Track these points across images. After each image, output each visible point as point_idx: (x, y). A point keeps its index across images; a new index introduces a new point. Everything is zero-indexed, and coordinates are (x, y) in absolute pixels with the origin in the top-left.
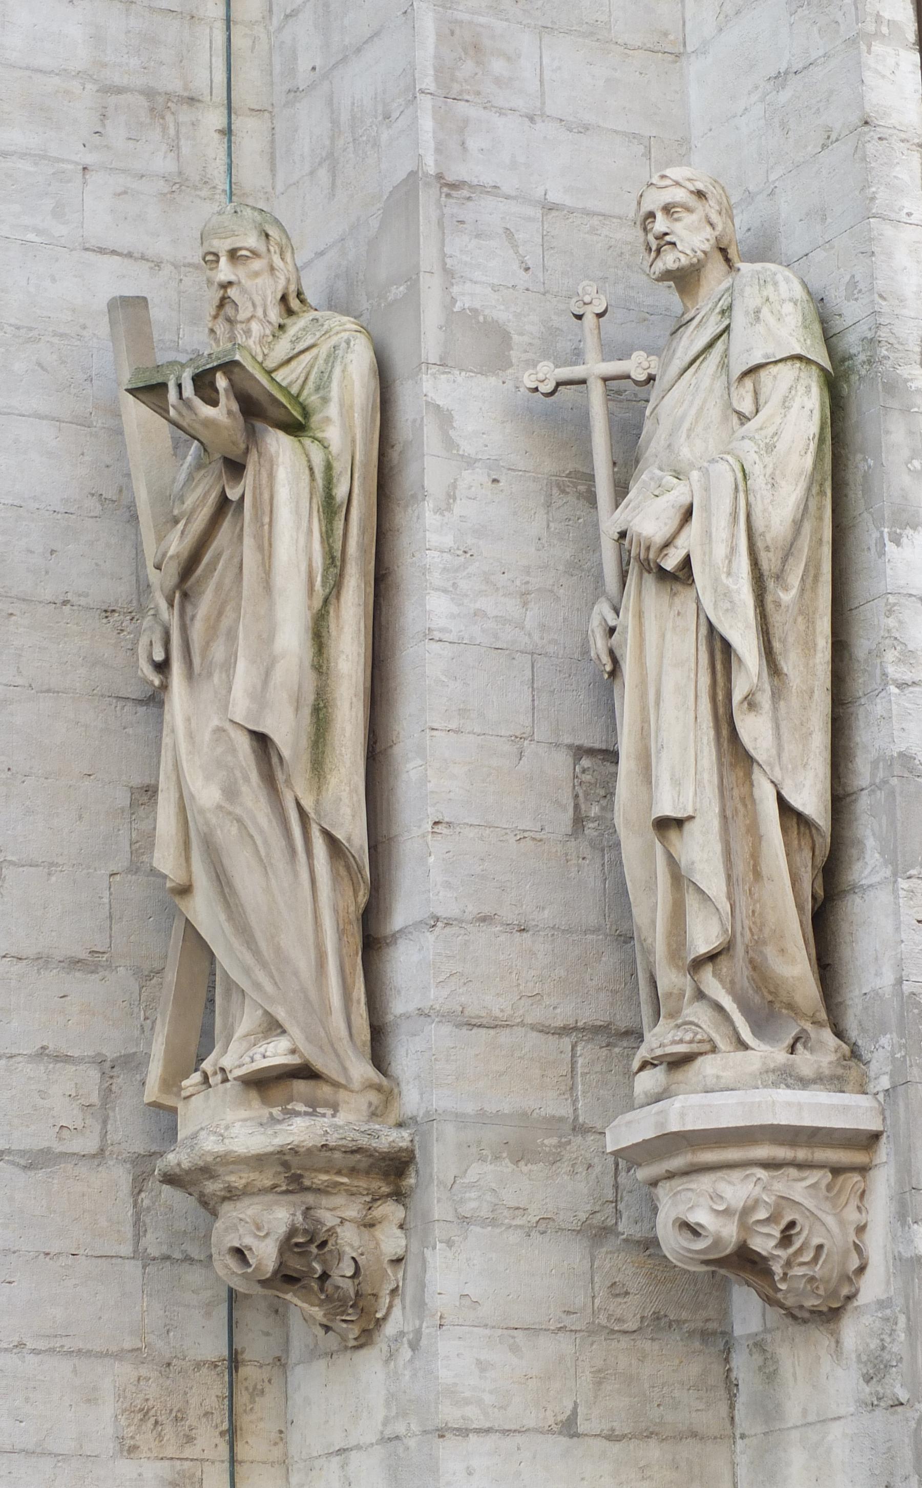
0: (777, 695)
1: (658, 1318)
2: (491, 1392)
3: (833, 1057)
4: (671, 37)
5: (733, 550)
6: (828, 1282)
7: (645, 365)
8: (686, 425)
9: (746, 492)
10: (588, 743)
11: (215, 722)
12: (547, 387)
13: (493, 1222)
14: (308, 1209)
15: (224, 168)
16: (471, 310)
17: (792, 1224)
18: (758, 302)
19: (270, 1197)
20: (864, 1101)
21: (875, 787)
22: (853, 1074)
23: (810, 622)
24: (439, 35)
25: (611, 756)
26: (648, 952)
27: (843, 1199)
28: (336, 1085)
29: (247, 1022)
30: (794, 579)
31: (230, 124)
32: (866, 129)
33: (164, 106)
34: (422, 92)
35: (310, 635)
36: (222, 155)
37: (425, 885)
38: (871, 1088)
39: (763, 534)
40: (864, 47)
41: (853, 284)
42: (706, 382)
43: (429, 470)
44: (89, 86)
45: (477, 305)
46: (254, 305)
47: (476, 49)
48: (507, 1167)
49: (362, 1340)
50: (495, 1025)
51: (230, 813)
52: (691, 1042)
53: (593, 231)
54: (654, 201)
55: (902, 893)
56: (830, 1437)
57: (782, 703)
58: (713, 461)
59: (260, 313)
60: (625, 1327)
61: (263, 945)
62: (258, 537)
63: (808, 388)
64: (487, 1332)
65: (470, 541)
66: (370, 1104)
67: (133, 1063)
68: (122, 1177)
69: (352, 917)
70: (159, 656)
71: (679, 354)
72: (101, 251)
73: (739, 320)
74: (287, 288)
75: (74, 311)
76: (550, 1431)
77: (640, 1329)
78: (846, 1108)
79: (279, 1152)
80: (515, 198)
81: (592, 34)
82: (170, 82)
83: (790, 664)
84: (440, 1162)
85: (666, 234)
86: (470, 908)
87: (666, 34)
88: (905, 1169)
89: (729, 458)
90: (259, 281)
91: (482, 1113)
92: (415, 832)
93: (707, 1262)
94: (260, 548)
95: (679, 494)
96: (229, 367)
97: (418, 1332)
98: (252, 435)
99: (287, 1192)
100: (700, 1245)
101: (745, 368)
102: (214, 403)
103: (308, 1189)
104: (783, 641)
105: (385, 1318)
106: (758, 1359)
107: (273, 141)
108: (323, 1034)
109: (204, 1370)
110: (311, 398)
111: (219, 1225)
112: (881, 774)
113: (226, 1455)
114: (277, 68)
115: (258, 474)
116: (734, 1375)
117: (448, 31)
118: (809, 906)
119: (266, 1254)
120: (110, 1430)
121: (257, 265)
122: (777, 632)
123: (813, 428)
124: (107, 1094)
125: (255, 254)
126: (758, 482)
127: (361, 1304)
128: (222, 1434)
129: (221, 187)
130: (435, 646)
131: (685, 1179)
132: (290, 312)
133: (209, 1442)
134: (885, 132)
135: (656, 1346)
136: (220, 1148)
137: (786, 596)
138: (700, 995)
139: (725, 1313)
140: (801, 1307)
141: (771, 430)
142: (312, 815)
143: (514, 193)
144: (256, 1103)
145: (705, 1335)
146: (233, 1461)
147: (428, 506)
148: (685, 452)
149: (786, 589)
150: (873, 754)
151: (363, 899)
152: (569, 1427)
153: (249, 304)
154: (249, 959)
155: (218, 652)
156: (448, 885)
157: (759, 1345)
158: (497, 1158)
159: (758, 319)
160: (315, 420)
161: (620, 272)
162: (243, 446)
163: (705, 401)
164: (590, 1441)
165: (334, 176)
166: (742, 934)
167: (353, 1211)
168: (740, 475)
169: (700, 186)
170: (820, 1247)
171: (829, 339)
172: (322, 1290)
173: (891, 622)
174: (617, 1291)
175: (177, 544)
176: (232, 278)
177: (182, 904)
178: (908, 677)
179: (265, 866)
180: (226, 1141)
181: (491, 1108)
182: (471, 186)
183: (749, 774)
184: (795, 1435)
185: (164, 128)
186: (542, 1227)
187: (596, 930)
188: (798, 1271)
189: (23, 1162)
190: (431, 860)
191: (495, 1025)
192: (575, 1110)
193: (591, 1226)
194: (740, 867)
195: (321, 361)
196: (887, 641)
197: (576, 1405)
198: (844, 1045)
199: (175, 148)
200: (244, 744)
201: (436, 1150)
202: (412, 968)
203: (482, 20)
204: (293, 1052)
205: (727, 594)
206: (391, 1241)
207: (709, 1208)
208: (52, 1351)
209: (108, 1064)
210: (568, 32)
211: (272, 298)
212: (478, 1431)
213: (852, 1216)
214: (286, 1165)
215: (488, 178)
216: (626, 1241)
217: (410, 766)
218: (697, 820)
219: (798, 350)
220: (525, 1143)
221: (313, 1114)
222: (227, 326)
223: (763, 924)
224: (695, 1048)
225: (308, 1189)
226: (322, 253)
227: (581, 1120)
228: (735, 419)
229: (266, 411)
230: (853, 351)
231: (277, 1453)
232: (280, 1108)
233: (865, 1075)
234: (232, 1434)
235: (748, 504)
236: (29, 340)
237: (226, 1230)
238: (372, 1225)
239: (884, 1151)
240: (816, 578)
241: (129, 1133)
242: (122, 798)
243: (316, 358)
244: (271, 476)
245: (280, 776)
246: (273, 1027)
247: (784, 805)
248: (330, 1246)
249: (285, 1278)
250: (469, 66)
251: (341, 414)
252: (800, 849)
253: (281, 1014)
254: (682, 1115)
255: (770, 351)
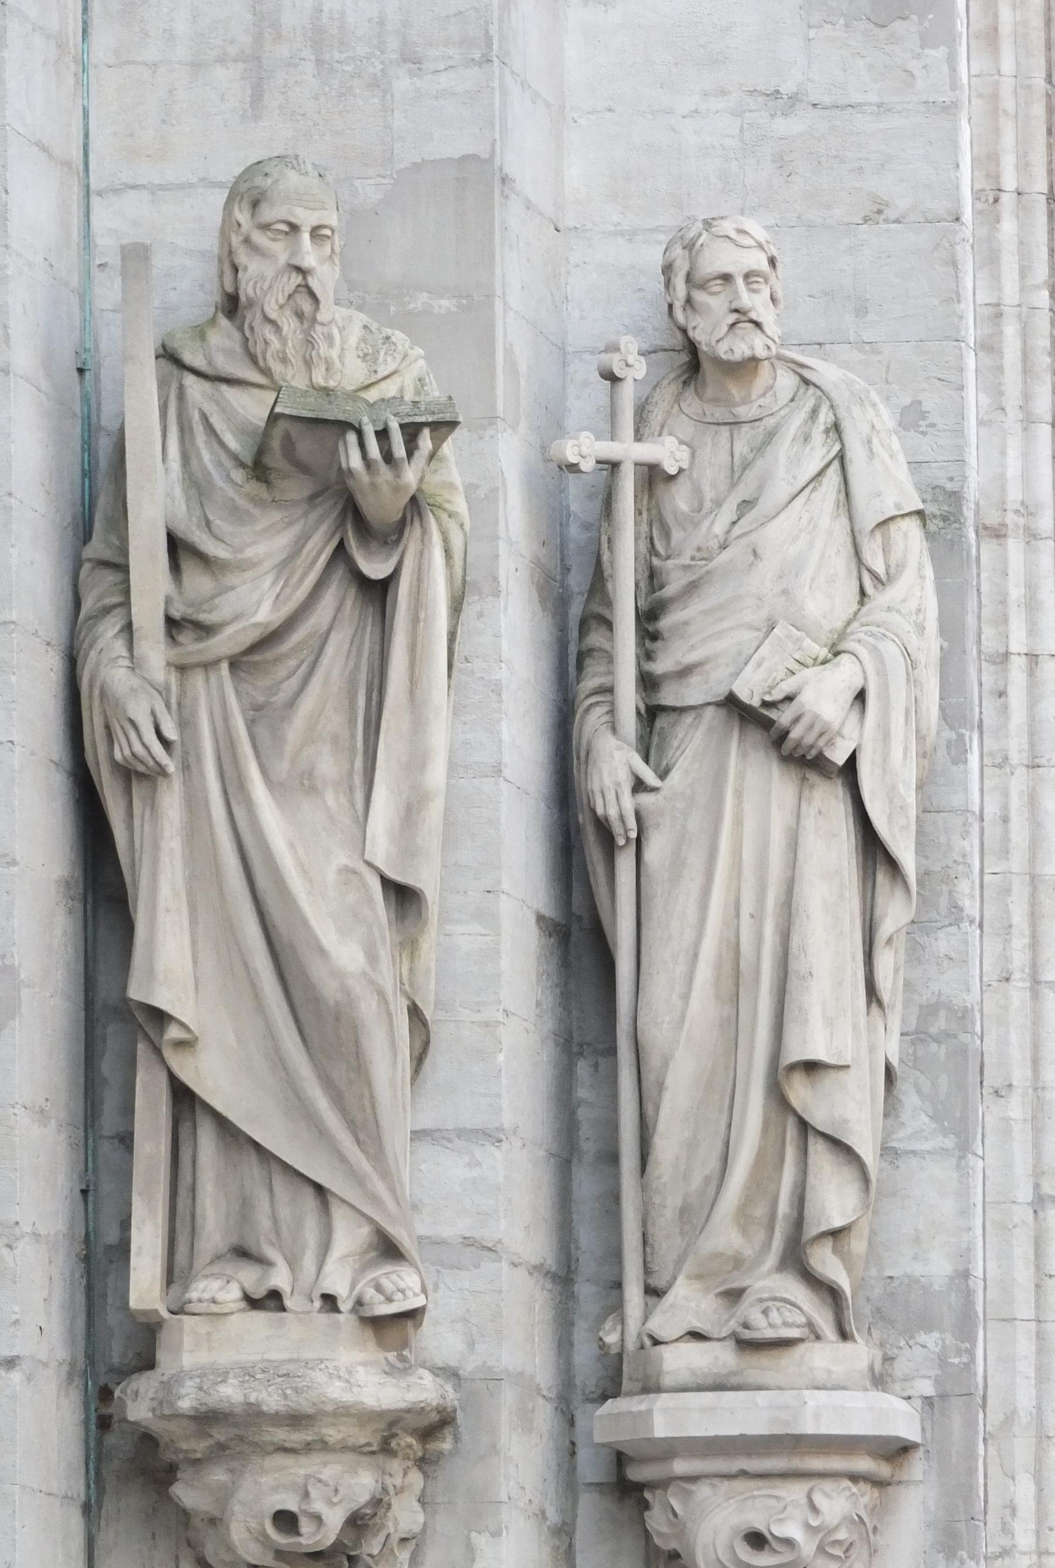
136: (347, 1398)
144: (371, 1344)
180: (355, 1389)
190: (501, 1058)
196: (961, 868)
218: (852, 1071)
232: (395, 1354)
239: (917, 1467)
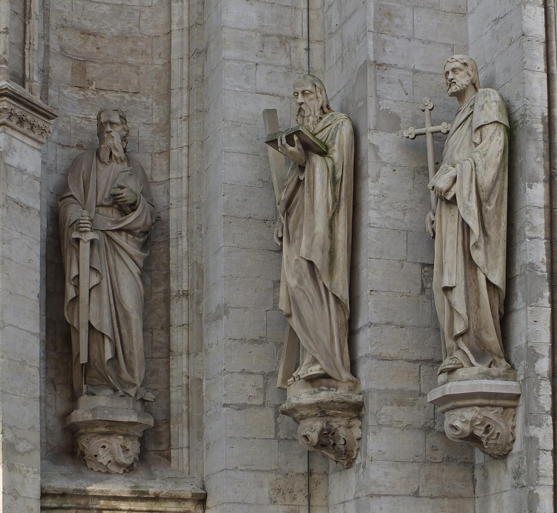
0: (486, 243)
1: (449, 458)
2: (389, 483)
3: (504, 369)
4: (462, 8)
5: (470, 192)
6: (502, 445)
7: (446, 127)
8: (457, 148)
9: (476, 171)
10: (426, 262)
11: (296, 258)
12: (412, 136)
13: (390, 426)
14: (328, 422)
15: (307, 62)
16: (386, 109)
17: (489, 426)
18: (483, 102)
19: (315, 418)
20: (514, 384)
21: (521, 275)
22: (512, 375)
23: (499, 217)
24: (375, 10)
25: (432, 265)
26: (444, 334)
27: (507, 417)
28: (337, 380)
29: (307, 359)
30: (493, 202)
31: (309, 46)
32: (523, 37)
33: (285, 40)
34: (369, 31)
35: (328, 226)
36: (306, 58)
37: (368, 312)
38: (518, 379)
39: (481, 186)
40: (523, 7)
41: (518, 94)
42: (464, 132)
43: (370, 167)
44: (258, 34)
45: (388, 108)
46: (311, 111)
47: (389, 15)
48: (396, 407)
49: (349, 466)
50: (392, 360)
51: (300, 289)
52: (455, 364)
53: (432, 79)
54: (449, 67)
55: (529, 312)
56: (503, 498)
57: (488, 246)
58: (465, 160)
59: (313, 113)
60: (436, 461)
61: (311, 333)
62: (309, 192)
63: (500, 133)
64: (388, 462)
65: (385, 192)
66: (349, 387)
67: (274, 374)
68: (270, 412)
69: (344, 324)
70: (280, 236)
71: (455, 122)
72: (263, 93)
73: (476, 109)
74: (323, 104)
75: (253, 115)
76: (410, 495)
77: (442, 462)
78: (507, 386)
79: (317, 403)
80: (403, 69)
81: (432, 8)
82: (288, 32)
83: (492, 232)
84: (372, 406)
85: (452, 79)
86: (383, 320)
87: (460, 7)
88: (527, 407)
89: (470, 159)
90: (313, 102)
91: (387, 389)
92: (365, 294)
93: (461, 439)
94: (310, 196)
95: (452, 172)
96: (298, 133)
97: (365, 463)
98: (307, 157)
99: (320, 416)
100: (458, 433)
101: (477, 127)
102: (294, 146)
103: (328, 415)
104: (489, 224)
105: (355, 458)
106: (482, 472)
107: (325, 52)
108: (332, 363)
109: (300, 476)
110: (329, 143)
111: (300, 428)
112: (523, 270)
113: (307, 504)
114: (326, 26)
115: (309, 171)
116: (475, 477)
117: (379, 9)
118: (498, 317)
119: (314, 437)
120: (267, 496)
121: (312, 96)
122: (486, 221)
123: (501, 147)
124: (266, 385)
125: (311, 92)
126: (480, 167)
127: (347, 454)
128: (306, 497)
129: (306, 69)
130: (372, 229)
131: (453, 411)
132: (324, 113)
133: (301, 499)
134: (530, 38)
135: (448, 467)
136: (297, 402)
137: (490, 208)
138: (458, 348)
139: (472, 457)
140: (494, 454)
141: (485, 149)
142: (329, 289)
143: (402, 67)
144: (310, 387)
145: (465, 464)
146: (309, 505)
147: (369, 181)
148: (456, 158)
149: (490, 205)
150: (520, 264)
151: (347, 317)
152: (416, 494)
153: (309, 111)
154: (307, 339)
155: (297, 233)
156: (375, 312)
157: (483, 467)
158: (392, 404)
159: (483, 109)
160: (330, 151)
161: (441, 94)
162: (304, 161)
163: (463, 139)
164: (424, 499)
165: (343, 63)
166: (473, 327)
167: (343, 422)
168: (473, 165)
169: (465, 61)
170: (499, 434)
171: (510, 115)
172: (334, 449)
173: (528, 216)
174: (434, 449)
175: (284, 196)
176: (303, 101)
177: (289, 320)
178: (533, 236)
179: (312, 306)
181: (390, 388)
182: (386, 65)
183: (476, 271)
184: (493, 497)
185: (285, 49)
186: (408, 427)
187: (429, 327)
188: (491, 442)
189: (237, 408)
190: (370, 303)
191: (392, 360)
192: (420, 388)
193: (425, 427)
194: (472, 304)
195: (333, 130)
196: (526, 223)
197: (419, 486)
198: (509, 365)
199: (289, 56)
200: (305, 264)
201: (370, 402)
202: (364, 340)
203: (391, 4)
204: (321, 369)
205: (468, 208)
206: (357, 433)
207: (460, 420)
208: (247, 470)
209: (266, 375)
210: (424, 7)
211: (317, 108)
212: (384, 495)
213: (510, 423)
214: (319, 407)
215: (393, 62)
216: (438, 432)
217: (363, 271)
219: (496, 119)
220: (401, 399)
221: (329, 390)
222: (302, 118)
223: (481, 323)
224: (456, 366)
225: (328, 415)
226: (339, 92)
227: (422, 391)
228: (473, 145)
229: (312, 148)
230: (518, 119)
231: (325, 503)
233: (516, 375)
234: (309, 497)
235: (476, 175)
236: (237, 126)
237: (302, 429)
238: (350, 427)
239: (521, 401)
240: (502, 201)
241: (272, 397)
242: (270, 285)
243: (331, 129)
244: (314, 171)
245: (318, 276)
246: (315, 361)
247: (488, 281)
248: (336, 434)
249: (321, 445)
250: (386, 21)
251: (339, 148)
252: (495, 297)
253: (317, 357)
254: (450, 389)
255: (486, 120)
